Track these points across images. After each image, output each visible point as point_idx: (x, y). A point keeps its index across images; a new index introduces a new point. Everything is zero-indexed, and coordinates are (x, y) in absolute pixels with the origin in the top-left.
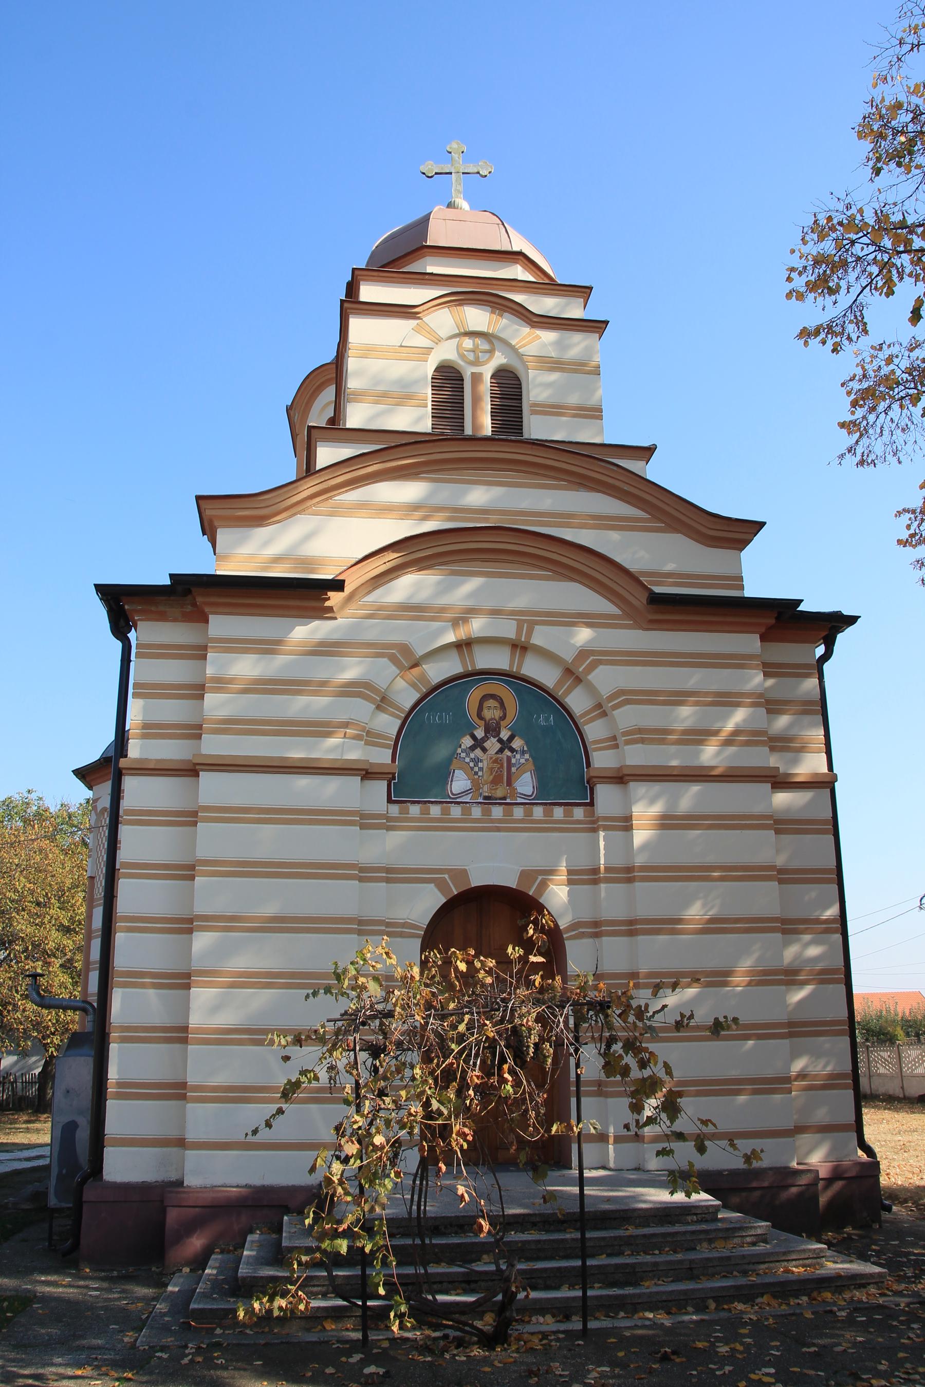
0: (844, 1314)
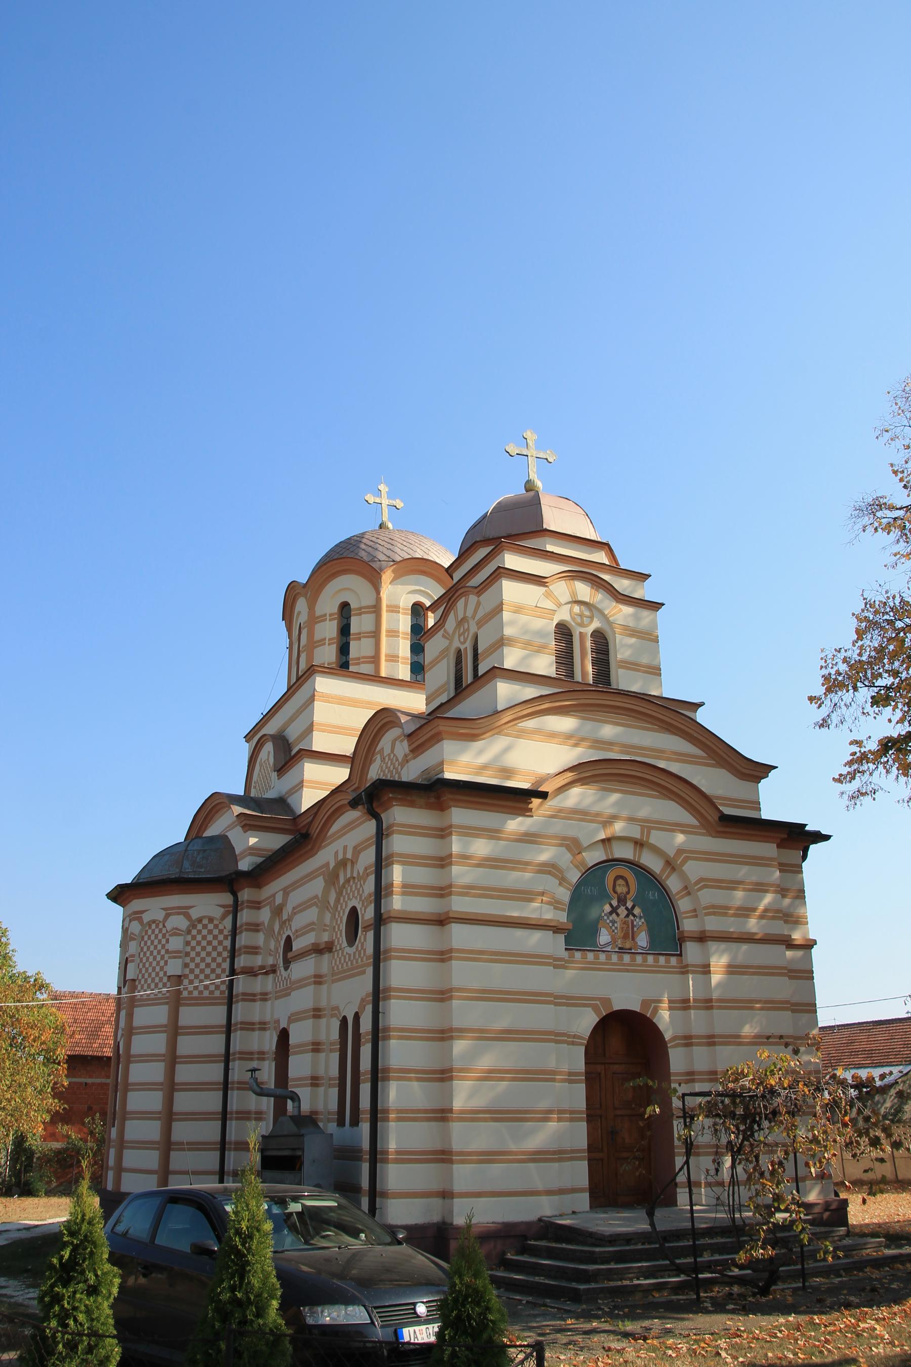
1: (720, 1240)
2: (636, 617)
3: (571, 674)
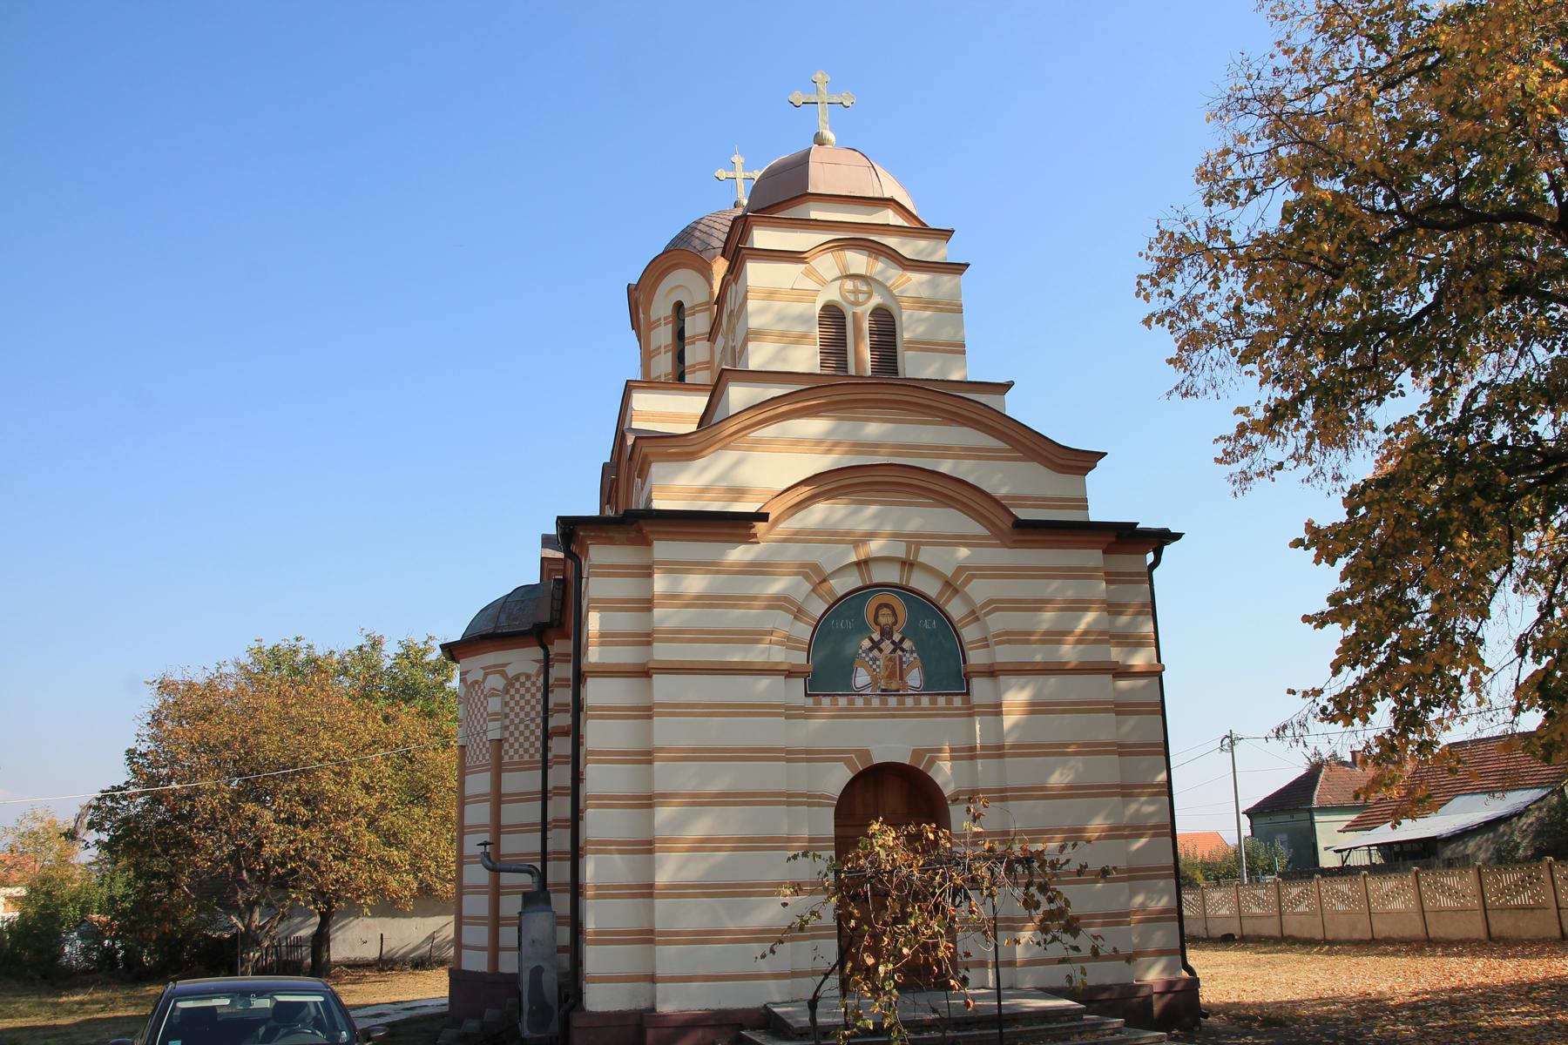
2: (934, 285)
3: (843, 365)
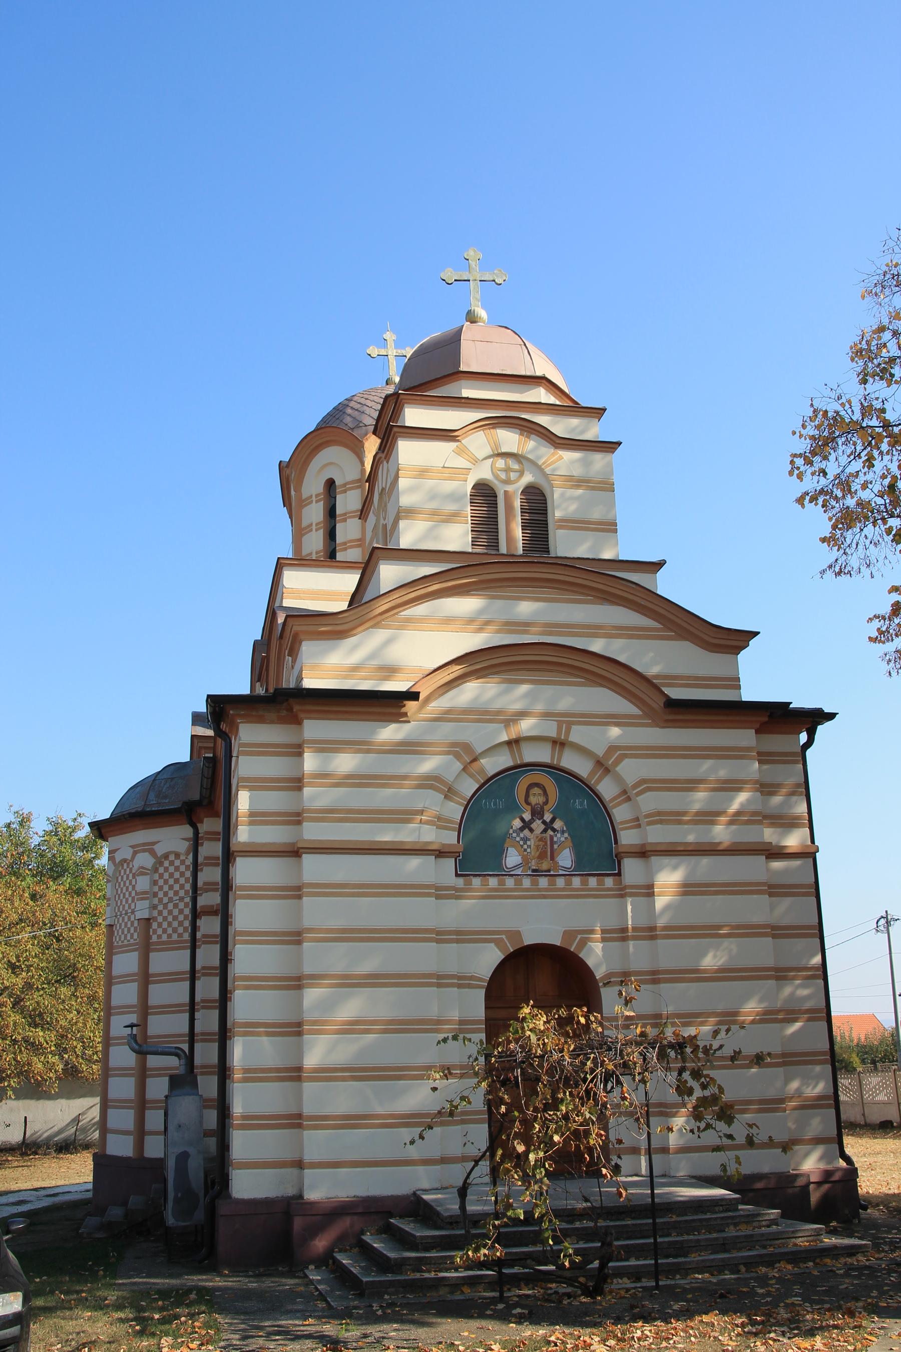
0: (842, 1272)
1: (587, 1224)
2: (586, 464)
3: (494, 543)
